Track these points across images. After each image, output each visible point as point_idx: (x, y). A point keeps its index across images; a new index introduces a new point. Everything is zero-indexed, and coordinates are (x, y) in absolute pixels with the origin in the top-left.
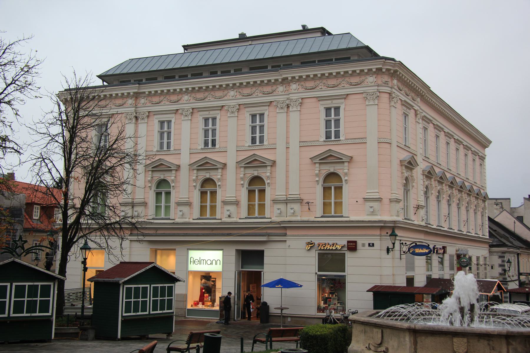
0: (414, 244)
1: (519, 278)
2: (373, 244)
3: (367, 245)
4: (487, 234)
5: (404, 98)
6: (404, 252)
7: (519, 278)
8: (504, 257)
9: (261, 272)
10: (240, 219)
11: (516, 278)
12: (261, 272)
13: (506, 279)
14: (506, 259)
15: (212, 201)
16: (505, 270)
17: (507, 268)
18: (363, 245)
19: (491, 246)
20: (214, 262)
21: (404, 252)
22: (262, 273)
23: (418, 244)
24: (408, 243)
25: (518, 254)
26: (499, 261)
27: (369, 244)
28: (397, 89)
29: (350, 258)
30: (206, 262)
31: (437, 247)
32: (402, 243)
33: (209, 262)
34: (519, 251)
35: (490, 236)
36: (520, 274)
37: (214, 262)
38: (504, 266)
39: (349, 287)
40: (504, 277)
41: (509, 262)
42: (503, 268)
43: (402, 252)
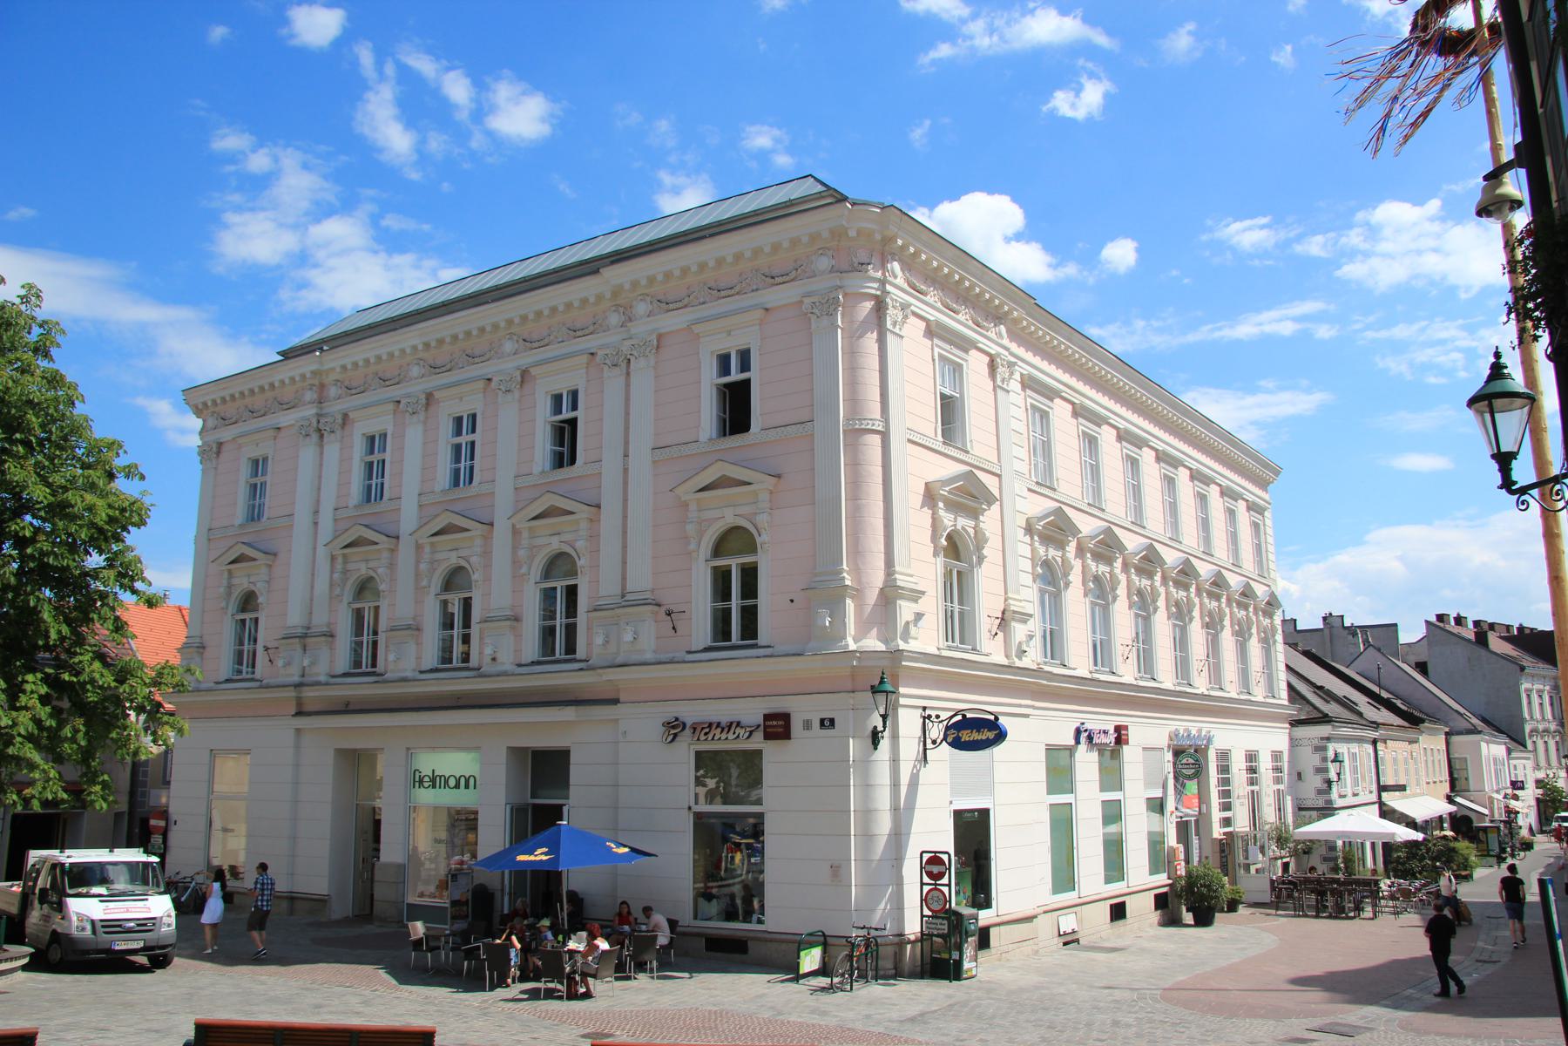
0: (959, 717)
1: (1380, 796)
2: (832, 721)
3: (816, 724)
4: (1284, 694)
5: (933, 315)
6: (934, 742)
7: (1380, 796)
8: (1325, 749)
9: (561, 806)
10: (689, 652)
11: (1374, 797)
12: (561, 806)
13: (1330, 802)
14: (1331, 755)
15: (726, 613)
16: (1329, 782)
17: (1333, 775)
18: (807, 725)
19: (1296, 723)
20: (463, 781)
21: (934, 742)
22: (565, 809)
23: (969, 715)
24: (944, 715)
25: (1374, 742)
26: (1315, 760)
27: (822, 721)
28: (906, 286)
29: (774, 757)
30: (446, 782)
31: (1088, 726)
32: (929, 717)
33: (452, 782)
34: (1373, 734)
35: (1291, 700)
36: (1382, 788)
37: (463, 781)
38: (1326, 770)
39: (771, 841)
40: (1326, 797)
41: (1337, 759)
42: (1324, 775)
43: (929, 741)
